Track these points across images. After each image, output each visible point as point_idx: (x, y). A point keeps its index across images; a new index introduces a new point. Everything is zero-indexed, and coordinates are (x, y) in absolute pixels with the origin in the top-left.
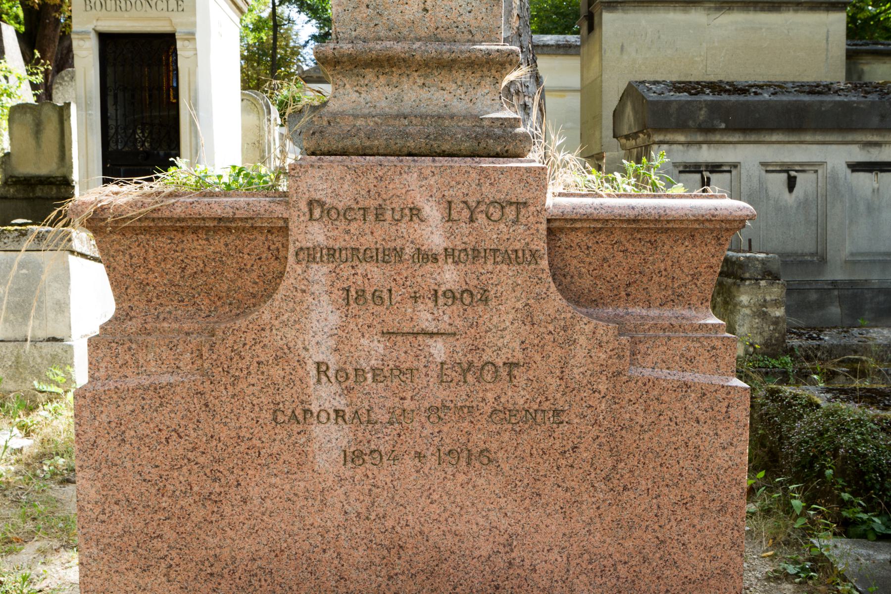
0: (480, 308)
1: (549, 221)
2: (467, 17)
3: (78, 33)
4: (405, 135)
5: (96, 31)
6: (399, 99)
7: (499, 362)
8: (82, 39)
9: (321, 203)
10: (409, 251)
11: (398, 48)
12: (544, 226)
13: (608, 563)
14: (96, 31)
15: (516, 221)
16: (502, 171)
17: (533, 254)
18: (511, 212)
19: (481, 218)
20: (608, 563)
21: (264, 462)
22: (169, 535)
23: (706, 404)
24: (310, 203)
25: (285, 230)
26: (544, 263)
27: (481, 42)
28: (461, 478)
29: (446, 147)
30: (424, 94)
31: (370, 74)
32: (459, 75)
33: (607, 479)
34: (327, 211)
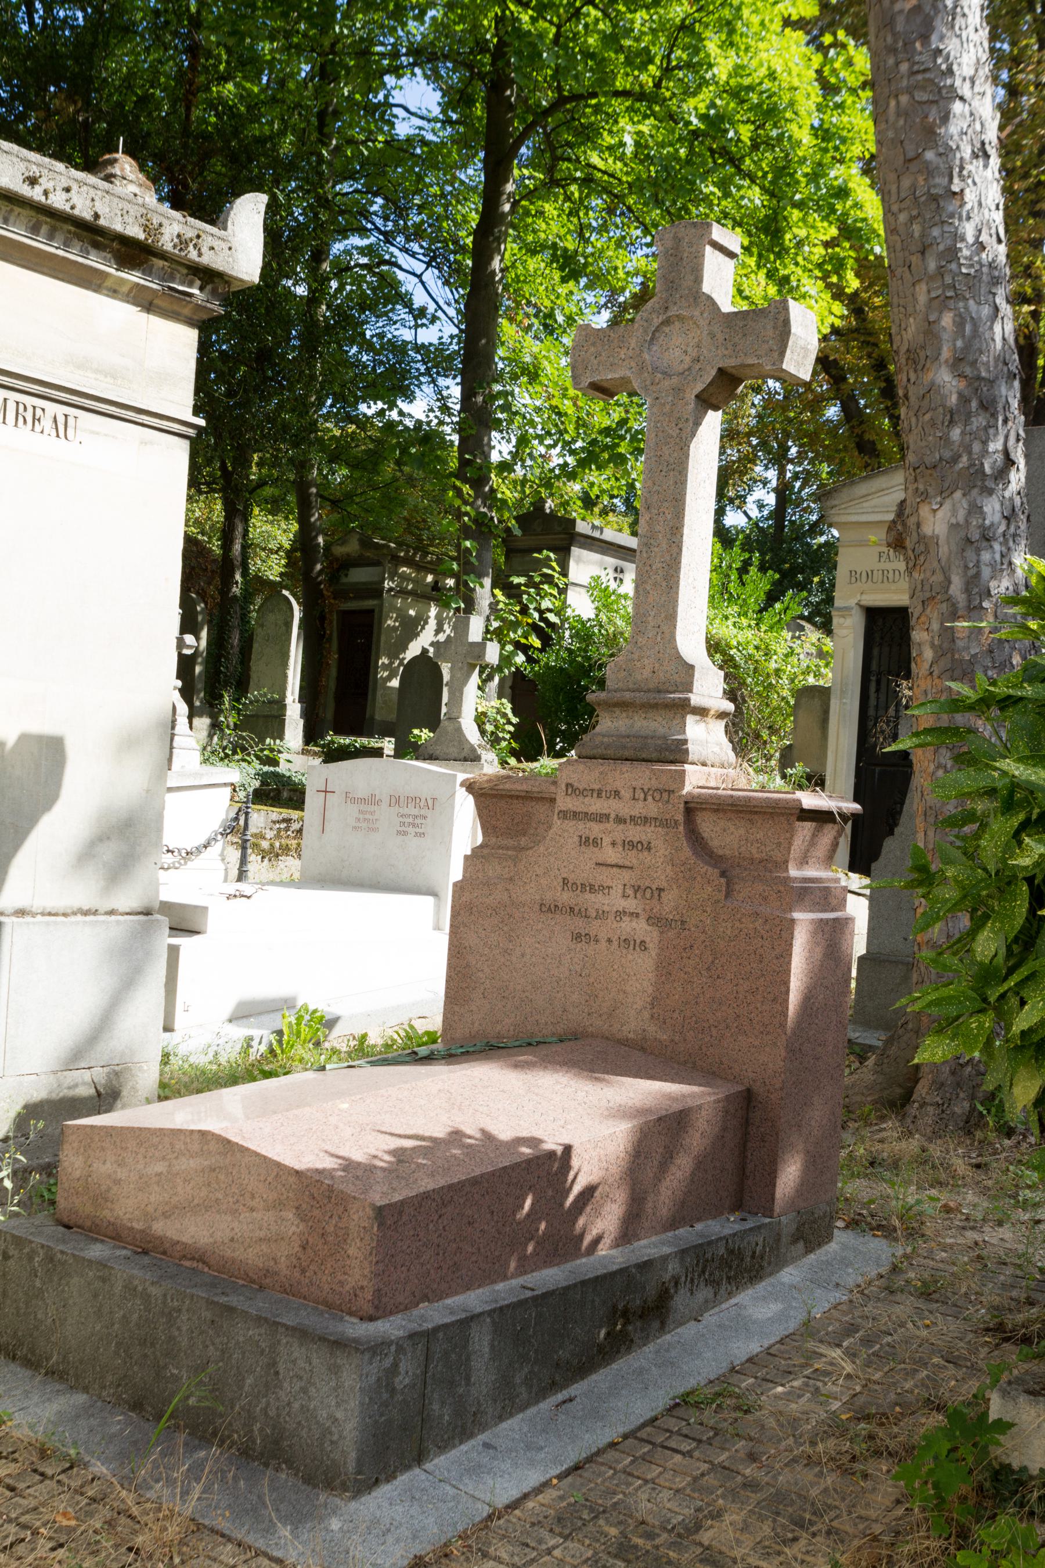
0: (646, 853)
1: (686, 803)
2: (676, 676)
3: (839, 609)
4: (624, 747)
5: (861, 606)
6: (632, 726)
7: (654, 887)
8: (843, 616)
9: (572, 786)
10: (613, 816)
11: (628, 695)
12: (682, 806)
13: (706, 1025)
14: (861, 606)
15: (668, 802)
16: (662, 771)
17: (676, 822)
18: (665, 795)
19: (650, 798)
20: (706, 1025)
21: (1011, 1168)
22: (487, 970)
23: (767, 927)
24: (567, 785)
25: (553, 800)
26: (681, 828)
27: (674, 692)
28: (630, 957)
29: (644, 756)
30: (645, 723)
31: (617, 711)
32: (663, 712)
33: (708, 969)
34: (574, 790)
